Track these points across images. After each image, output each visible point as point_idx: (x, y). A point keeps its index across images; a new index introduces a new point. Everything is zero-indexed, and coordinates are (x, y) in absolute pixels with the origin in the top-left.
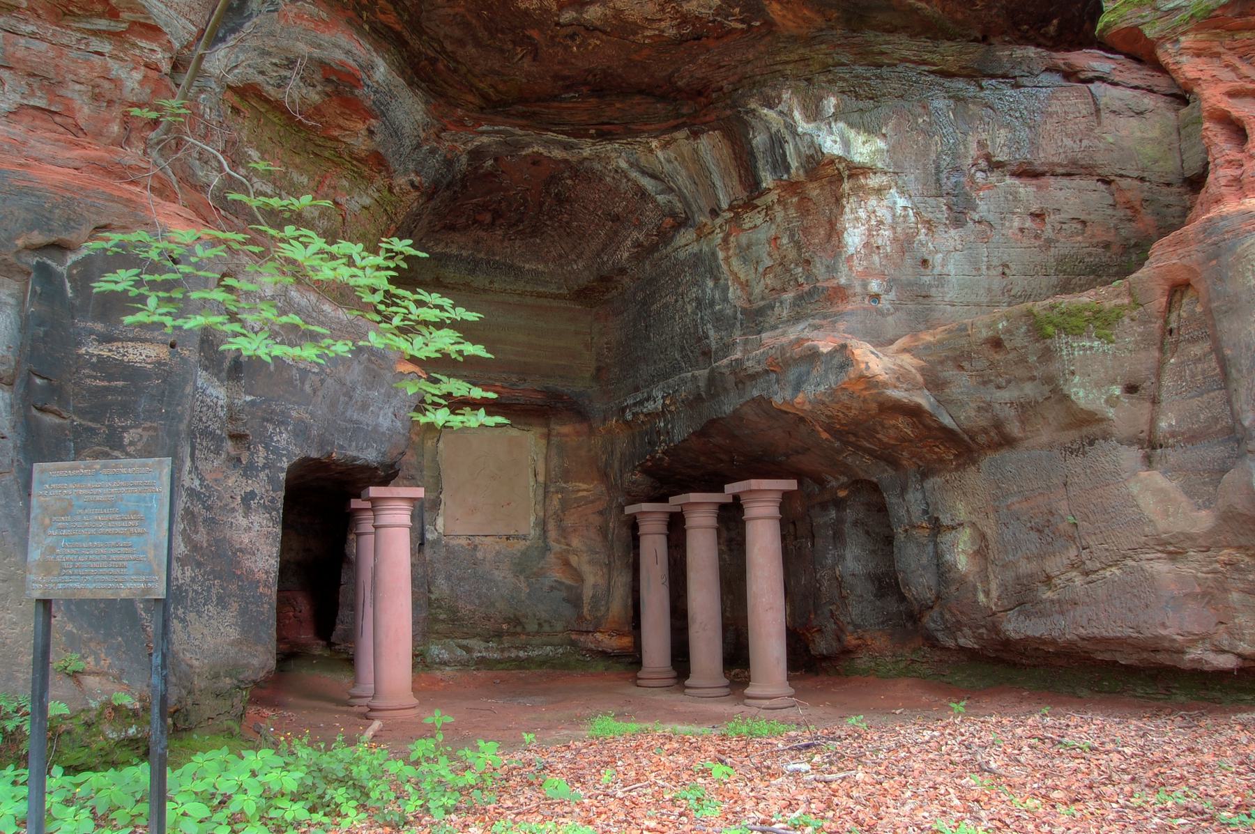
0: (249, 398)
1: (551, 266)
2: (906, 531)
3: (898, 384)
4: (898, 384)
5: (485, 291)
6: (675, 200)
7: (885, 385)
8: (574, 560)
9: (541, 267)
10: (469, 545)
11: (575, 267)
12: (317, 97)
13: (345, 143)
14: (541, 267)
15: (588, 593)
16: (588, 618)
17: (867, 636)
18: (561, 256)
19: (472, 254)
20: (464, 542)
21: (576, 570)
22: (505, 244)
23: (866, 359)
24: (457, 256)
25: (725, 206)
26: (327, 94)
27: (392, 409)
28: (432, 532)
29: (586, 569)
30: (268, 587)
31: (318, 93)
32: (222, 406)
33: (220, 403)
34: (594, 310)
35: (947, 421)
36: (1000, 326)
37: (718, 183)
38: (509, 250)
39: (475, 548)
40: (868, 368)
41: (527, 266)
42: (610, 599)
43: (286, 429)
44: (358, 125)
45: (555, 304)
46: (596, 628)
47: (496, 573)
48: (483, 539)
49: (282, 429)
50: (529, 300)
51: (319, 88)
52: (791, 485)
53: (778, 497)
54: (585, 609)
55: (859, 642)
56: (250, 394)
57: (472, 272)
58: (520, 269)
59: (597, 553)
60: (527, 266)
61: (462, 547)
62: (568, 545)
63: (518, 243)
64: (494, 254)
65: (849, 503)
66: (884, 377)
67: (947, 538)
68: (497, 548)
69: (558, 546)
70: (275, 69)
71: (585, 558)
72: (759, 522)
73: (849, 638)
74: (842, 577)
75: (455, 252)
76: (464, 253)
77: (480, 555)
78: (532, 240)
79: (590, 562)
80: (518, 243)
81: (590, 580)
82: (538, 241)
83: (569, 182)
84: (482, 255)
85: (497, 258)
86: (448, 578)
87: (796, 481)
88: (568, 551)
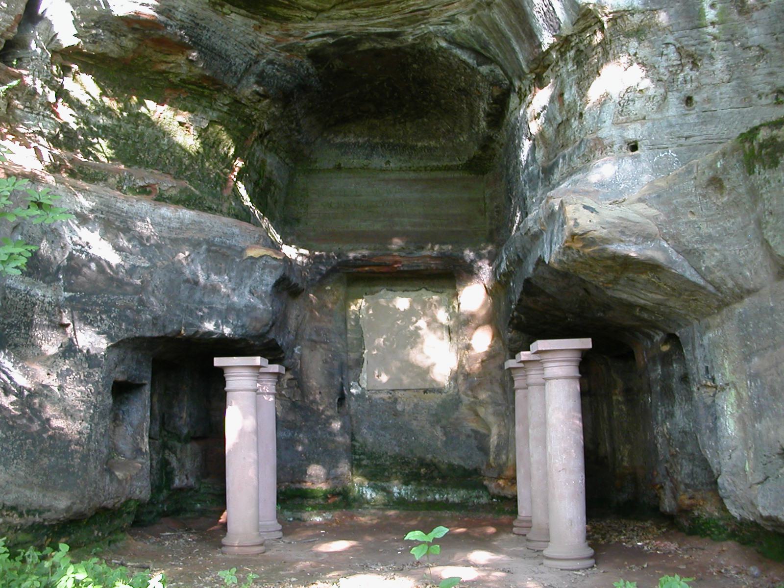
0: (67, 294)
1: (443, 141)
2: (698, 389)
3: (623, 238)
4: (623, 238)
5: (382, 170)
6: (499, 71)
7: (606, 241)
8: (481, 411)
9: (433, 143)
10: (390, 398)
11: (462, 139)
12: (132, 43)
13: (174, 73)
14: (433, 143)
15: (494, 440)
16: (493, 465)
17: (698, 496)
18: (448, 131)
19: (368, 140)
20: (385, 396)
21: (483, 420)
22: (398, 127)
23: (576, 216)
24: (354, 144)
25: (526, 70)
26: (138, 39)
27: (248, 289)
28: (356, 388)
29: (491, 419)
30: (80, 445)
31: (131, 40)
32: (49, 303)
33: (47, 300)
34: (485, 177)
35: (690, 274)
36: (719, 166)
37: (517, 48)
38: (401, 132)
39: (396, 401)
40: (576, 224)
41: (420, 144)
42: (509, 448)
43: (109, 317)
44: (179, 58)
45: (449, 175)
46: (499, 475)
47: (415, 423)
48: (402, 392)
49: (104, 317)
50: (423, 175)
51: (130, 36)
52: (586, 343)
53: (577, 356)
54: (491, 457)
55: (692, 501)
56: (69, 291)
57: (368, 157)
58: (413, 148)
59: (500, 405)
60: (420, 144)
61: (384, 400)
62: (475, 397)
63: (408, 125)
64: (389, 138)
65: (674, 357)
66: (601, 233)
67: (721, 396)
68: (415, 400)
69: (467, 398)
70: (87, 30)
71: (491, 410)
72: (553, 382)
73: (683, 497)
74: (670, 434)
75: (353, 140)
76: (361, 140)
77: (399, 408)
78: (420, 120)
79: (496, 414)
80: (408, 125)
81: (494, 430)
82: (425, 120)
83: (415, 66)
84: (377, 140)
85: (392, 141)
86: (371, 427)
87: (590, 339)
88: (475, 403)
